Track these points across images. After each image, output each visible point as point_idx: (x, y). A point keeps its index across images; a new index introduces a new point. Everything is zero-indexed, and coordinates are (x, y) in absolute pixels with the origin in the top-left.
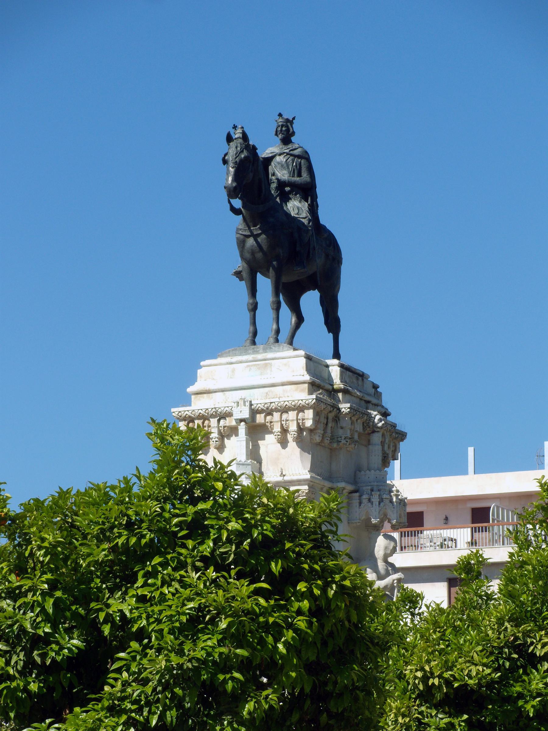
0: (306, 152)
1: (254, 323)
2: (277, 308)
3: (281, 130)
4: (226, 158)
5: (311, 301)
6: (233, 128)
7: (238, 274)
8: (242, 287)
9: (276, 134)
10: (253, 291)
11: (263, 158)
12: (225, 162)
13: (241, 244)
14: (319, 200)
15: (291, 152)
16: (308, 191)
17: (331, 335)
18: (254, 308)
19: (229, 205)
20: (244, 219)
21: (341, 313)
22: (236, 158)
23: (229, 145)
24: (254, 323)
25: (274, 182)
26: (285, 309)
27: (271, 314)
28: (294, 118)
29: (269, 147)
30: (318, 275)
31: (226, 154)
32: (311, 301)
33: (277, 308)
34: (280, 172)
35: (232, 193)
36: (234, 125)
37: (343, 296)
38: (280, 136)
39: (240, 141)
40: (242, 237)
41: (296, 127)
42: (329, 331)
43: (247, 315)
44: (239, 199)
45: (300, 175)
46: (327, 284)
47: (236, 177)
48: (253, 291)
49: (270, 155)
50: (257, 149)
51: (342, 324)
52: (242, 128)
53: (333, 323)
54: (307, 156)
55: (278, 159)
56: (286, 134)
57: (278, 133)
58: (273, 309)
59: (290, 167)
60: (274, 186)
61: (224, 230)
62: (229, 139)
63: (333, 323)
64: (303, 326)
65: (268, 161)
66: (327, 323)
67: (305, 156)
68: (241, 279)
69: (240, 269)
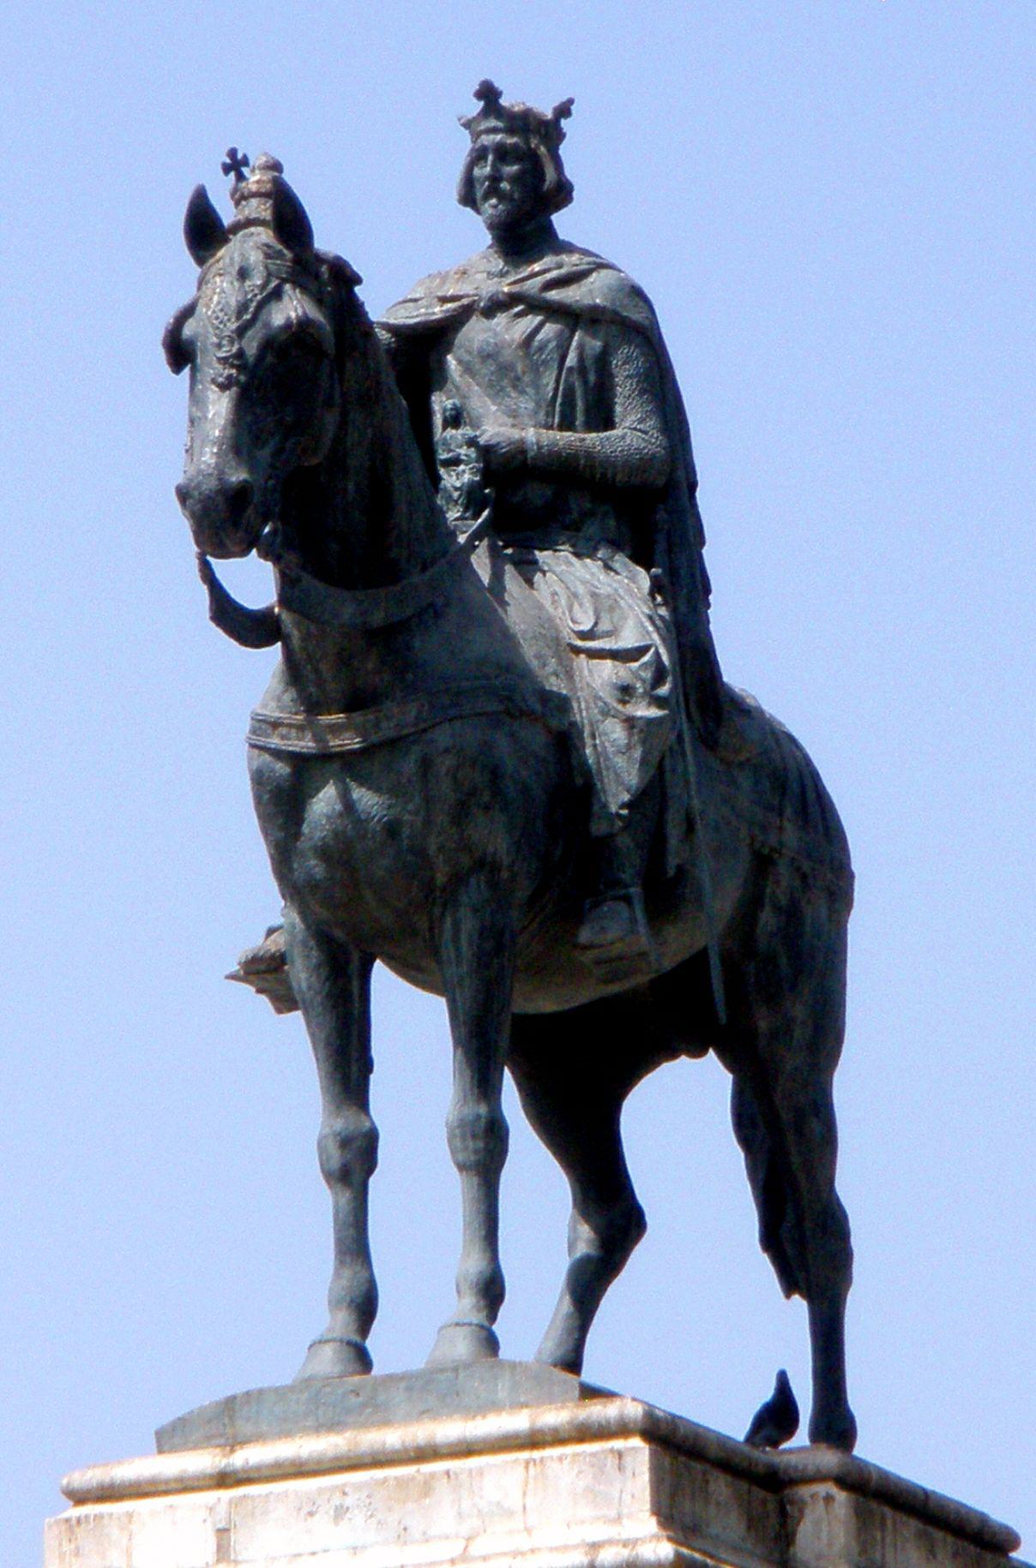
0: (637, 293)
1: (354, 1242)
2: (485, 1154)
3: (495, 179)
4: (188, 330)
5: (679, 1120)
6: (227, 169)
7: (264, 971)
8: (290, 1043)
9: (468, 198)
10: (348, 1061)
11: (394, 330)
12: (180, 352)
13: (282, 803)
14: (711, 555)
15: (554, 295)
16: (651, 515)
17: (800, 1304)
18: (354, 1163)
19: (204, 590)
20: (294, 671)
21: (853, 1182)
22: (241, 332)
23: (200, 261)
24: (354, 1242)
25: (456, 462)
26: (536, 1176)
27: (452, 1190)
28: (564, 110)
29: (412, 251)
30: (715, 960)
31: (188, 312)
32: (679, 1120)
33: (485, 1154)
34: (489, 414)
35: (222, 520)
36: (232, 153)
37: (853, 1089)
38: (491, 206)
39: (265, 235)
40: (282, 769)
41: (577, 157)
42: (790, 1284)
43: (321, 1205)
44: (265, 555)
45: (602, 418)
46: (769, 1005)
47: (248, 432)
48: (348, 1061)
49: (438, 312)
50: (357, 280)
51: (857, 1241)
52: (276, 167)
53: (806, 1240)
54: (637, 316)
55: (476, 332)
56: (521, 180)
57: (479, 194)
58: (462, 1167)
59: (549, 380)
60: (455, 480)
61: (173, 712)
62: (204, 232)
63: (806, 1240)
64: (640, 1257)
65: (425, 346)
66: (772, 1240)
67: (629, 329)
68: (285, 1001)
69: (278, 943)
